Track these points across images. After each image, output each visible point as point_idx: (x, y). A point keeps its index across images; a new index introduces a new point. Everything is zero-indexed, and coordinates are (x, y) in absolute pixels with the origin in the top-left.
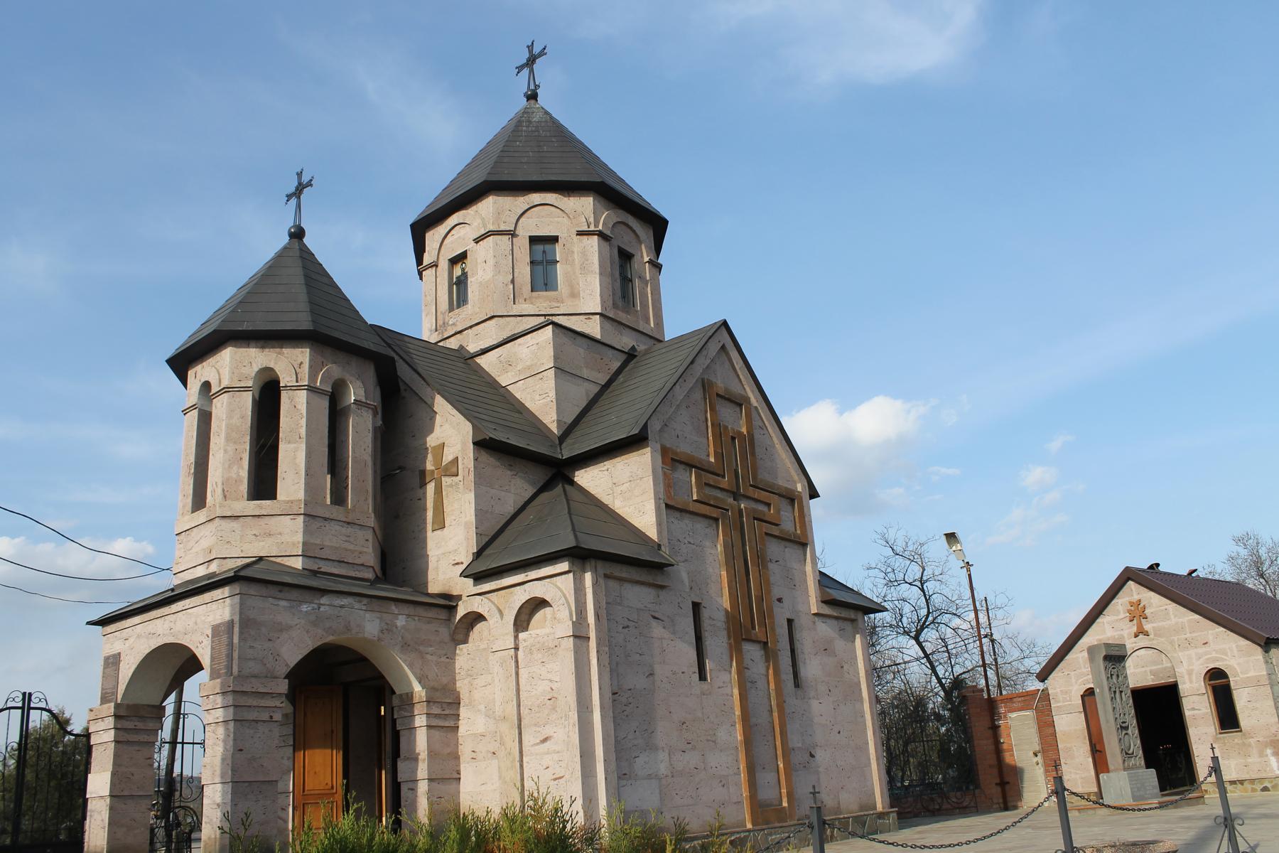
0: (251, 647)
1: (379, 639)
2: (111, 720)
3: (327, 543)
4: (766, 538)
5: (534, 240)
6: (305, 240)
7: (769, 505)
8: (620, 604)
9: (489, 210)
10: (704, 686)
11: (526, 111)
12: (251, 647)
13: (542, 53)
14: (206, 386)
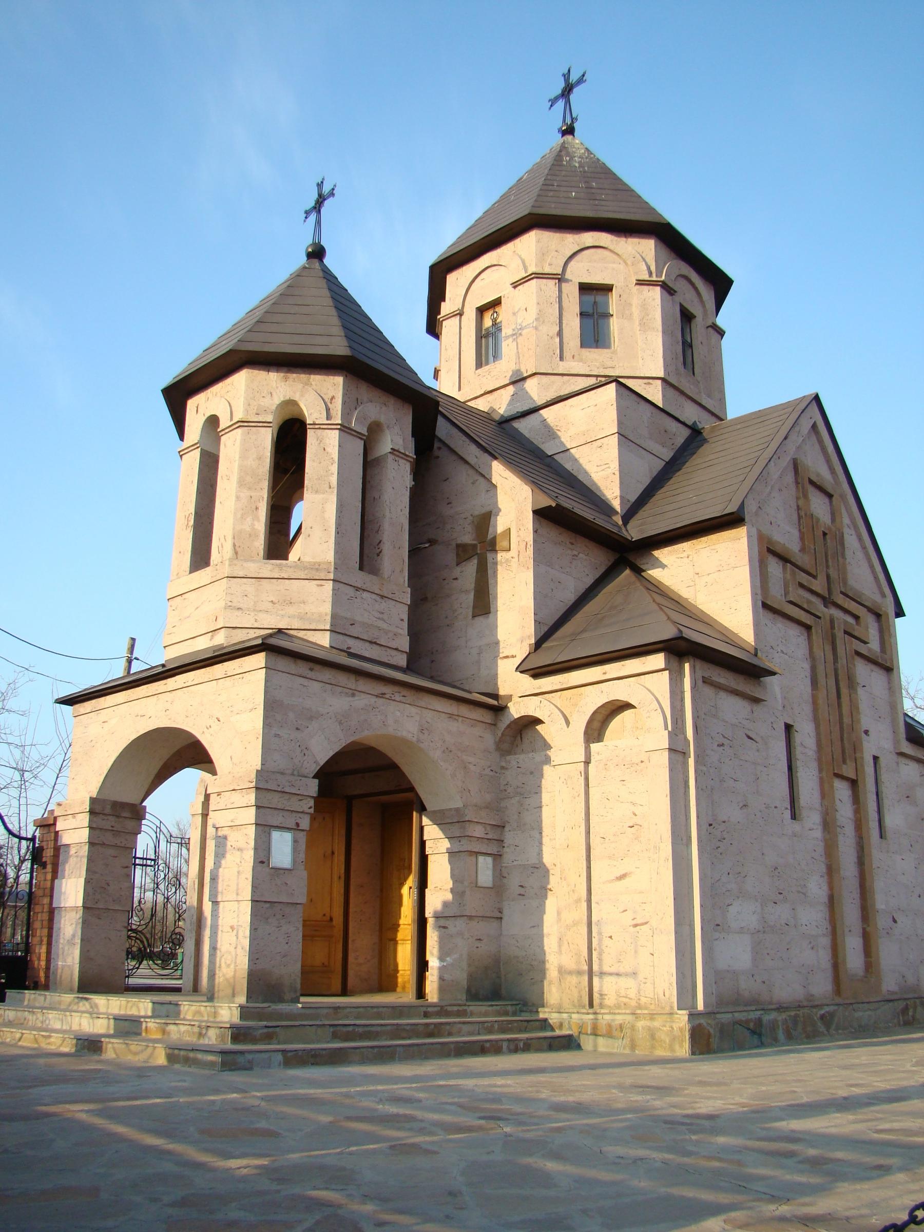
0: (277, 735)
1: (418, 741)
2: (86, 817)
3: (358, 618)
4: (856, 657)
5: (585, 288)
6: (326, 261)
7: (856, 618)
8: (715, 716)
9: (530, 248)
10: (796, 826)
11: (563, 147)
12: (277, 735)
13: (581, 80)
14: (213, 421)
